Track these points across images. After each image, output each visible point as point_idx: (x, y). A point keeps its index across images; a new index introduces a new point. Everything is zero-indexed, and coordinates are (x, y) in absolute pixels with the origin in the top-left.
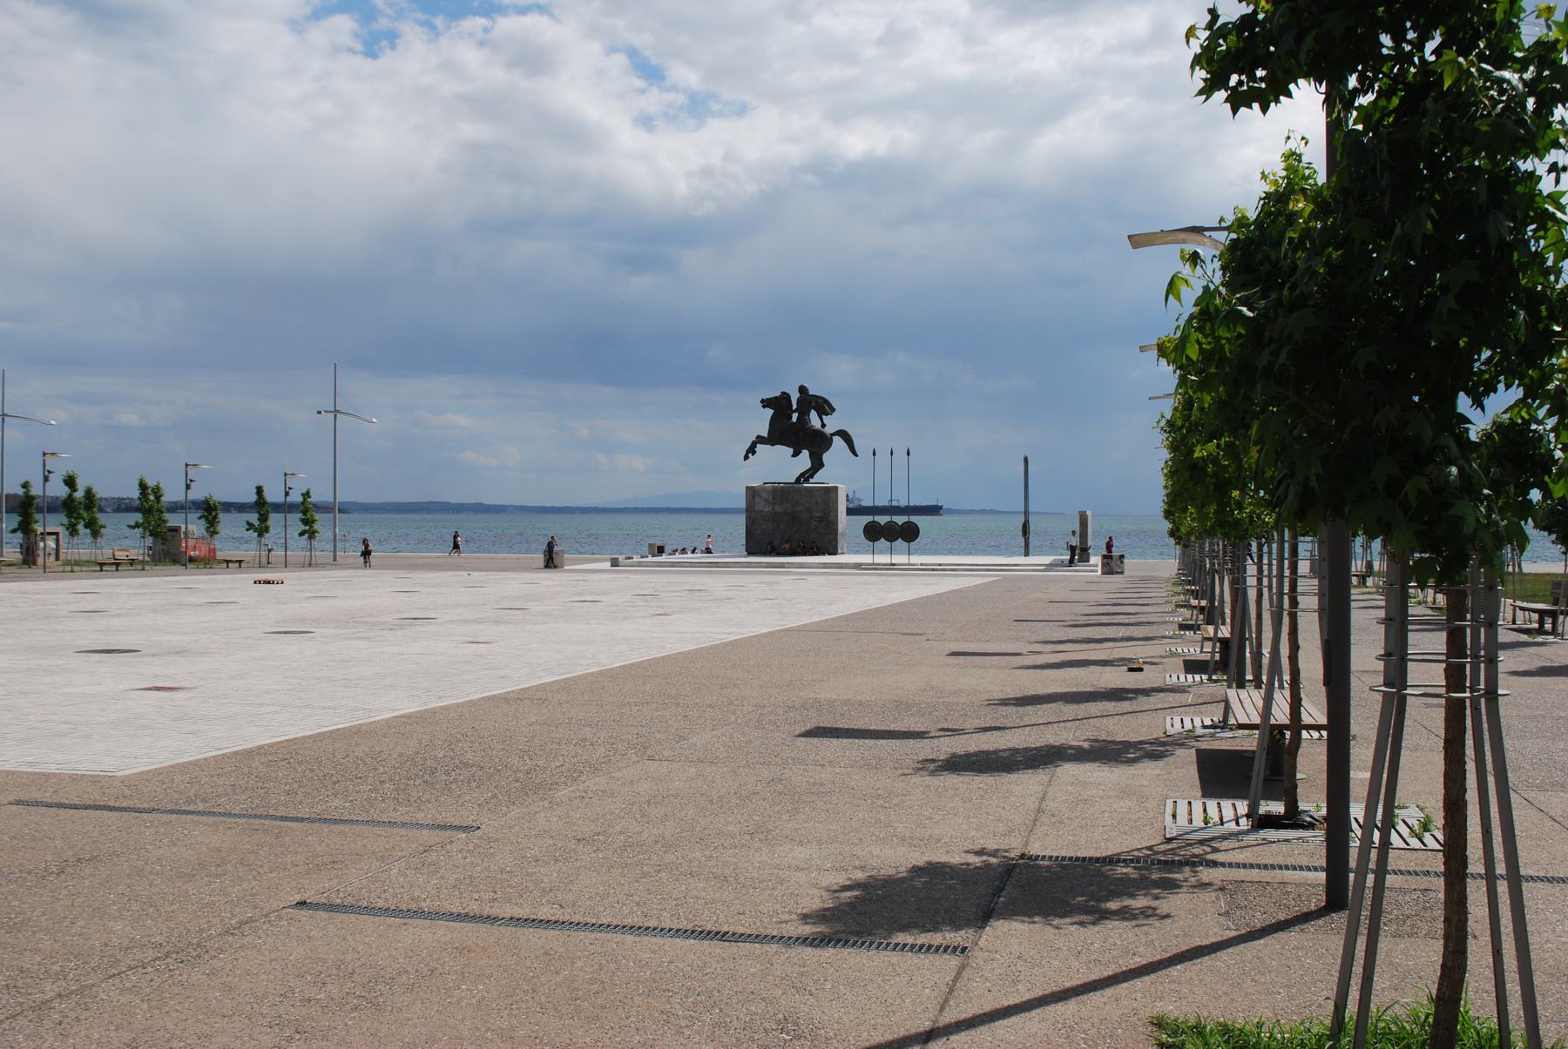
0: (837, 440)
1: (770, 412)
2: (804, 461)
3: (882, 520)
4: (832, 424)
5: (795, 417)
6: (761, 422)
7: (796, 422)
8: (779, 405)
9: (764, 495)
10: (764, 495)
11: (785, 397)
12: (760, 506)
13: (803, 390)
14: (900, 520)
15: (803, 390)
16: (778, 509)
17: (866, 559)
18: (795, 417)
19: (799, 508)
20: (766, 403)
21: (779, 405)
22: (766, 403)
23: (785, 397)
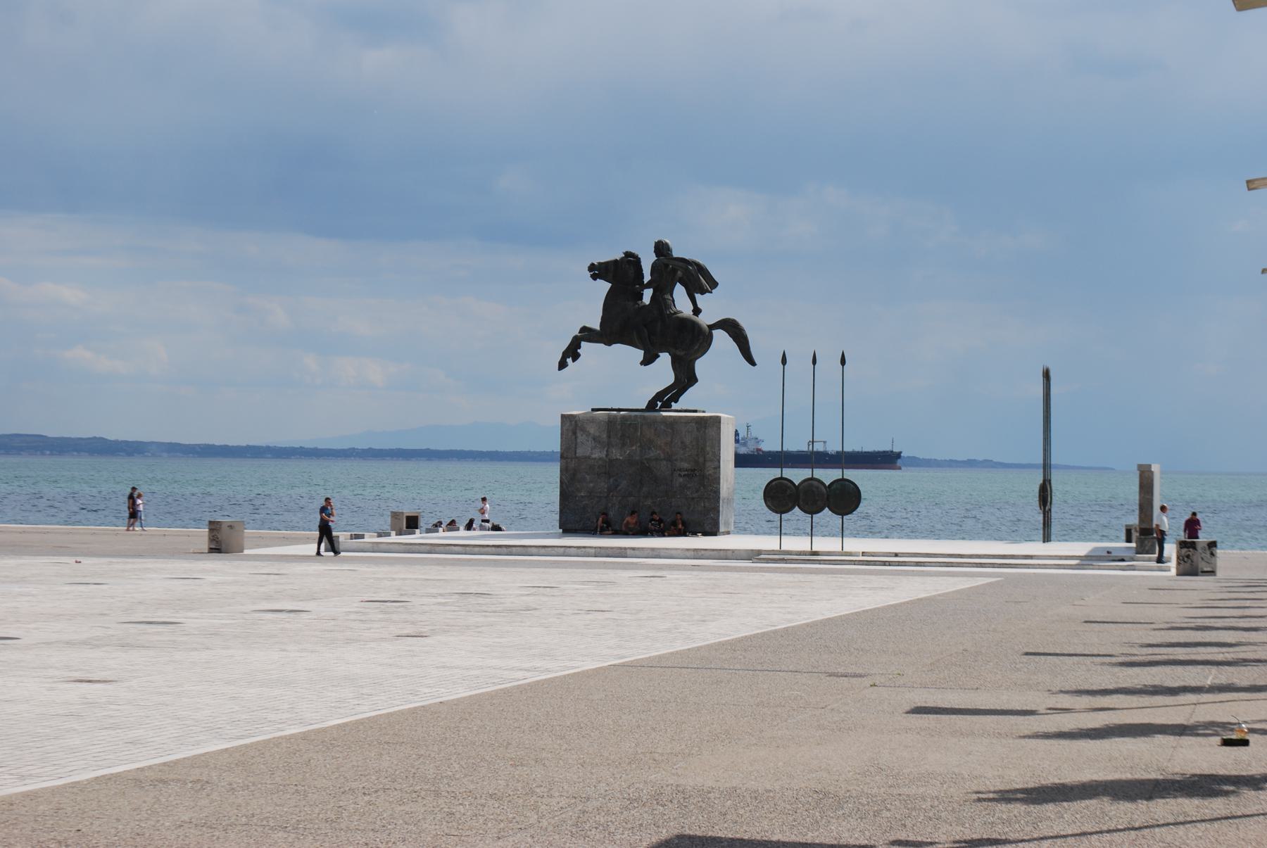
0: (720, 336)
1: (604, 287)
2: (663, 371)
3: (797, 475)
4: (711, 309)
5: (647, 295)
6: (590, 301)
7: (649, 305)
8: (619, 274)
9: (592, 430)
10: (592, 430)
11: (631, 260)
12: (586, 449)
13: (661, 249)
14: (828, 476)
15: (661, 249)
16: (616, 454)
17: (768, 543)
18: (647, 295)
19: (653, 453)
20: (598, 271)
21: (619, 274)
22: (598, 271)
23: (631, 260)
